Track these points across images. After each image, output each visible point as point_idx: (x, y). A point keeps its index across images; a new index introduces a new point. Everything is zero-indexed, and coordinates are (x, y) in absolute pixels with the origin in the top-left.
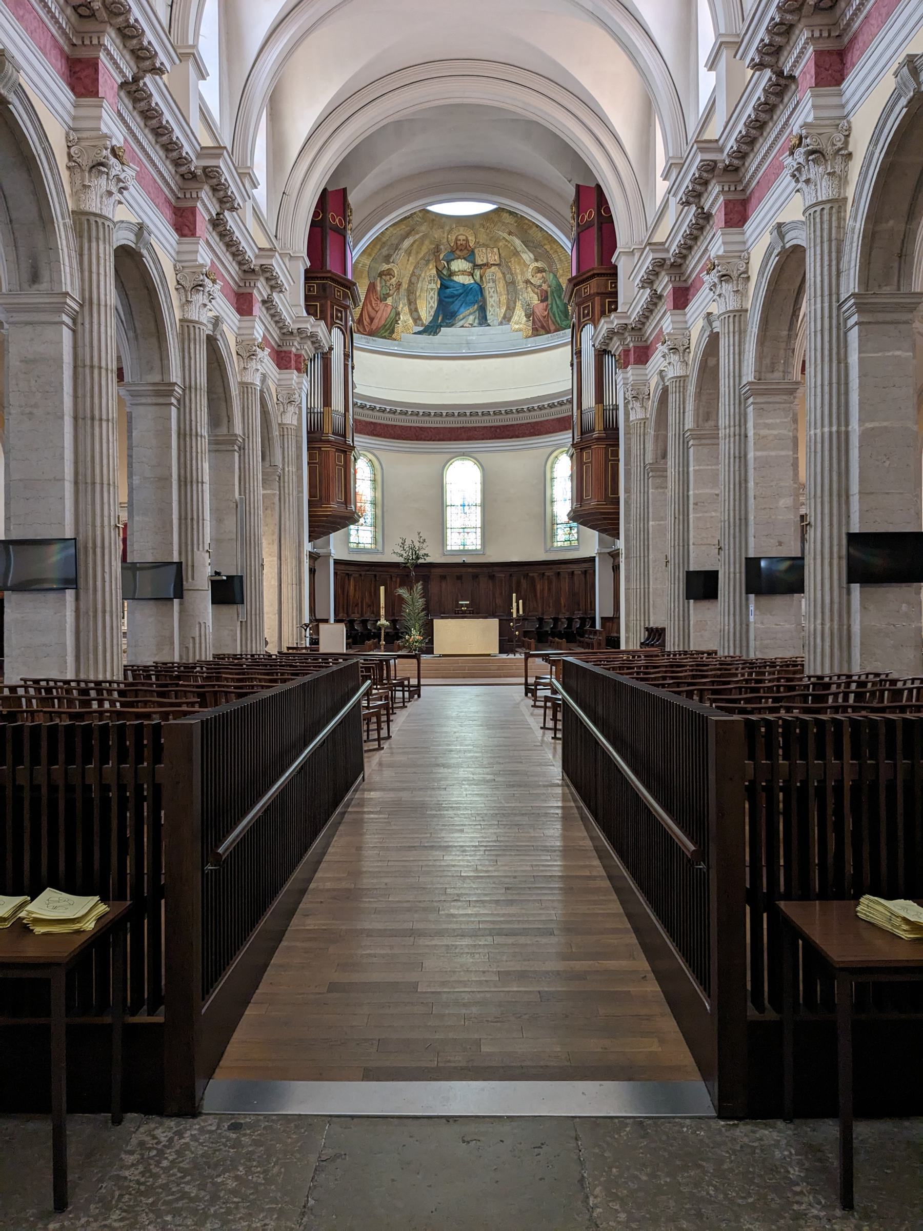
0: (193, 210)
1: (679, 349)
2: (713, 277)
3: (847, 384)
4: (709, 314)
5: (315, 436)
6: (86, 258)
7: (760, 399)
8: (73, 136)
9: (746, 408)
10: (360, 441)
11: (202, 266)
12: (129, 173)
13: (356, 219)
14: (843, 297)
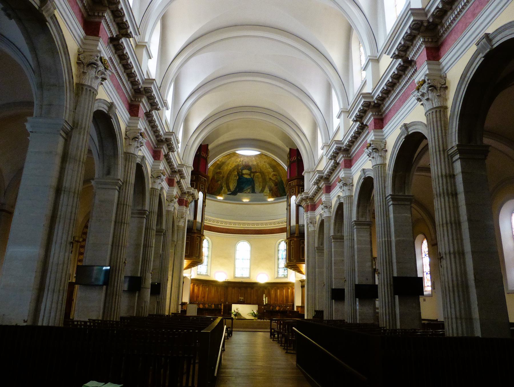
0: (160, 152)
1: (328, 207)
2: (341, 184)
3: (390, 224)
4: (339, 196)
5: (190, 230)
6: (127, 167)
7: (359, 227)
8: (128, 128)
9: (353, 229)
10: (205, 232)
11: (161, 170)
12: (144, 141)
13: (210, 154)
14: (387, 195)
